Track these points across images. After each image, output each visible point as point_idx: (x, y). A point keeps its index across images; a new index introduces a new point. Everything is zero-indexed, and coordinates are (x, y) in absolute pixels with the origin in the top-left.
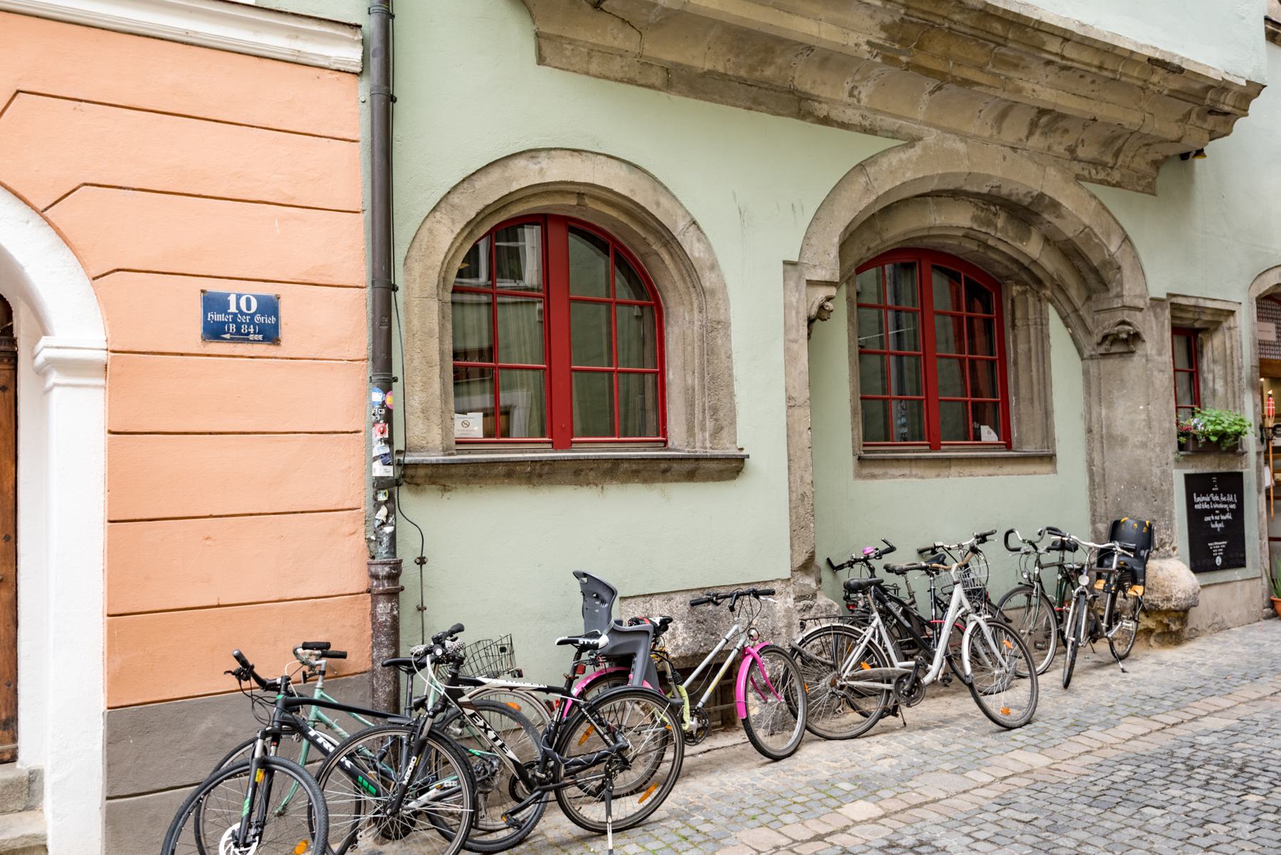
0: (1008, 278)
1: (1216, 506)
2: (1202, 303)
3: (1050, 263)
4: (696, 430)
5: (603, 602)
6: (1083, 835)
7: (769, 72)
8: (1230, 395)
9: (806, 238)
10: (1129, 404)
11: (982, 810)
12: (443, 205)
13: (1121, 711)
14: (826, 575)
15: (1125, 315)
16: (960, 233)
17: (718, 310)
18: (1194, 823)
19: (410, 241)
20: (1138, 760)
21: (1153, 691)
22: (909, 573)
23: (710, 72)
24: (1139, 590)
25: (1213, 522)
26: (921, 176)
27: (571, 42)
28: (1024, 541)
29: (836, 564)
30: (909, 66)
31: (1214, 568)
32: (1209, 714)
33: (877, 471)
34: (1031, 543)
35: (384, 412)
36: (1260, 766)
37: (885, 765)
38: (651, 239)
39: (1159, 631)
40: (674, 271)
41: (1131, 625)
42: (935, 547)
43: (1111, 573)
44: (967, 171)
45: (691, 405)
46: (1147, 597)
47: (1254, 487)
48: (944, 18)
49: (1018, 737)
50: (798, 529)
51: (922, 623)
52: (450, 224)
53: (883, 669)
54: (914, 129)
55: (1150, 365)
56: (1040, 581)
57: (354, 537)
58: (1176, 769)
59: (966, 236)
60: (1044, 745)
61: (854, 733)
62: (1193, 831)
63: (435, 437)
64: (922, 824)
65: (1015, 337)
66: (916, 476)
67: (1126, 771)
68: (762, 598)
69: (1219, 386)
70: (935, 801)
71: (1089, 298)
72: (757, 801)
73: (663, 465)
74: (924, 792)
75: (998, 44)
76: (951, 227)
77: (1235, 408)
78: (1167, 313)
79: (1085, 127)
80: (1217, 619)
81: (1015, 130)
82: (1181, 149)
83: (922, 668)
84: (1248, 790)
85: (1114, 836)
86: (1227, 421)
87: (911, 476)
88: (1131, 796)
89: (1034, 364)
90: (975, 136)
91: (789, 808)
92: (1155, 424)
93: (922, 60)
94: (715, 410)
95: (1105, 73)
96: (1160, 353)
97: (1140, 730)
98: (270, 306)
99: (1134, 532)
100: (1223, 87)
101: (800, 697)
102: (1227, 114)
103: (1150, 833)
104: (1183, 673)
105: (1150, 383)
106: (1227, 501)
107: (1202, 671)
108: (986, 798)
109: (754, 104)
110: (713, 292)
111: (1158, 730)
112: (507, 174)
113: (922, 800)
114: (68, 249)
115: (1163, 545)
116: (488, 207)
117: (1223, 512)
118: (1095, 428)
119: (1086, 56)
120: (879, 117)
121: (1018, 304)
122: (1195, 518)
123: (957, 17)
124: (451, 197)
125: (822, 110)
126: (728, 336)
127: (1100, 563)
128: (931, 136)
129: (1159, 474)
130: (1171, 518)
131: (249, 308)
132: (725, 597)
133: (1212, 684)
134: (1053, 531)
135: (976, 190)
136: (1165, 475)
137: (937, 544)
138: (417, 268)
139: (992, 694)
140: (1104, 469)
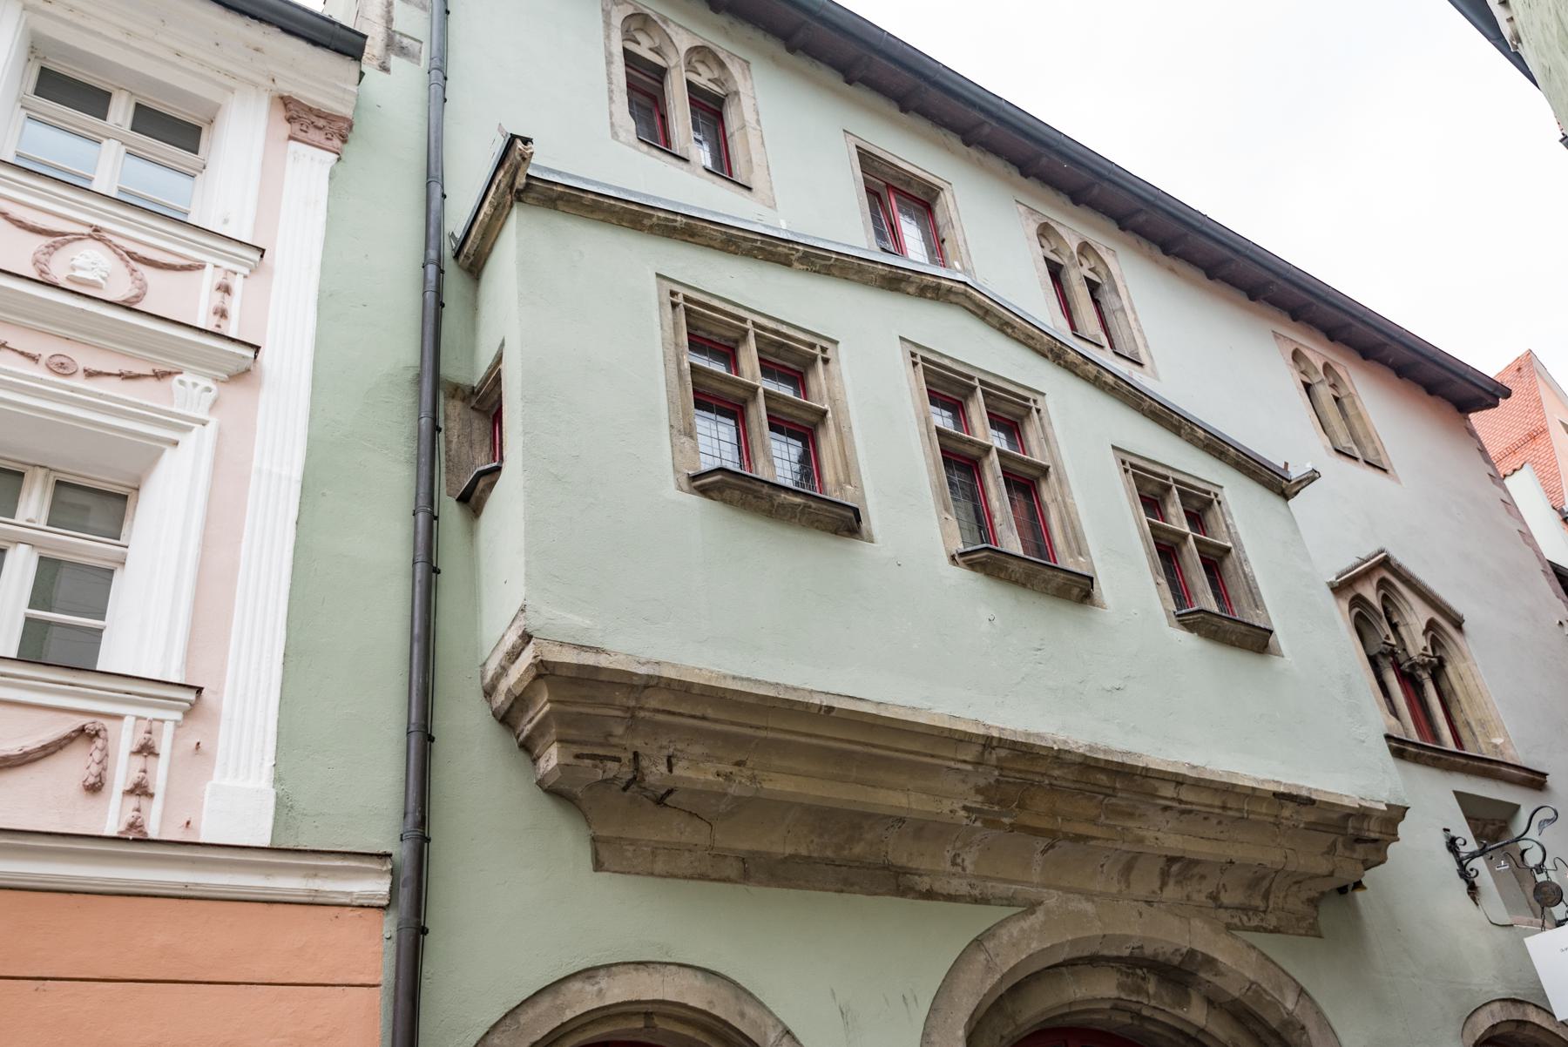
7: (858, 849)
23: (792, 857)
27: (632, 842)
30: (1013, 828)
44: (1100, 933)
48: (1043, 775)
54: (1032, 892)
59: (1114, 1008)
75: (1107, 795)
76: (1095, 1000)
79: (1222, 871)
82: (1336, 883)
90: (1101, 894)
93: (1027, 819)
95: (1230, 813)
100: (1363, 814)
102: (1375, 841)
109: (845, 886)
112: (558, 1002)
119: (1205, 798)
120: (989, 884)
123: (1056, 773)
124: (490, 1037)
125: (924, 883)
128: (1052, 899)
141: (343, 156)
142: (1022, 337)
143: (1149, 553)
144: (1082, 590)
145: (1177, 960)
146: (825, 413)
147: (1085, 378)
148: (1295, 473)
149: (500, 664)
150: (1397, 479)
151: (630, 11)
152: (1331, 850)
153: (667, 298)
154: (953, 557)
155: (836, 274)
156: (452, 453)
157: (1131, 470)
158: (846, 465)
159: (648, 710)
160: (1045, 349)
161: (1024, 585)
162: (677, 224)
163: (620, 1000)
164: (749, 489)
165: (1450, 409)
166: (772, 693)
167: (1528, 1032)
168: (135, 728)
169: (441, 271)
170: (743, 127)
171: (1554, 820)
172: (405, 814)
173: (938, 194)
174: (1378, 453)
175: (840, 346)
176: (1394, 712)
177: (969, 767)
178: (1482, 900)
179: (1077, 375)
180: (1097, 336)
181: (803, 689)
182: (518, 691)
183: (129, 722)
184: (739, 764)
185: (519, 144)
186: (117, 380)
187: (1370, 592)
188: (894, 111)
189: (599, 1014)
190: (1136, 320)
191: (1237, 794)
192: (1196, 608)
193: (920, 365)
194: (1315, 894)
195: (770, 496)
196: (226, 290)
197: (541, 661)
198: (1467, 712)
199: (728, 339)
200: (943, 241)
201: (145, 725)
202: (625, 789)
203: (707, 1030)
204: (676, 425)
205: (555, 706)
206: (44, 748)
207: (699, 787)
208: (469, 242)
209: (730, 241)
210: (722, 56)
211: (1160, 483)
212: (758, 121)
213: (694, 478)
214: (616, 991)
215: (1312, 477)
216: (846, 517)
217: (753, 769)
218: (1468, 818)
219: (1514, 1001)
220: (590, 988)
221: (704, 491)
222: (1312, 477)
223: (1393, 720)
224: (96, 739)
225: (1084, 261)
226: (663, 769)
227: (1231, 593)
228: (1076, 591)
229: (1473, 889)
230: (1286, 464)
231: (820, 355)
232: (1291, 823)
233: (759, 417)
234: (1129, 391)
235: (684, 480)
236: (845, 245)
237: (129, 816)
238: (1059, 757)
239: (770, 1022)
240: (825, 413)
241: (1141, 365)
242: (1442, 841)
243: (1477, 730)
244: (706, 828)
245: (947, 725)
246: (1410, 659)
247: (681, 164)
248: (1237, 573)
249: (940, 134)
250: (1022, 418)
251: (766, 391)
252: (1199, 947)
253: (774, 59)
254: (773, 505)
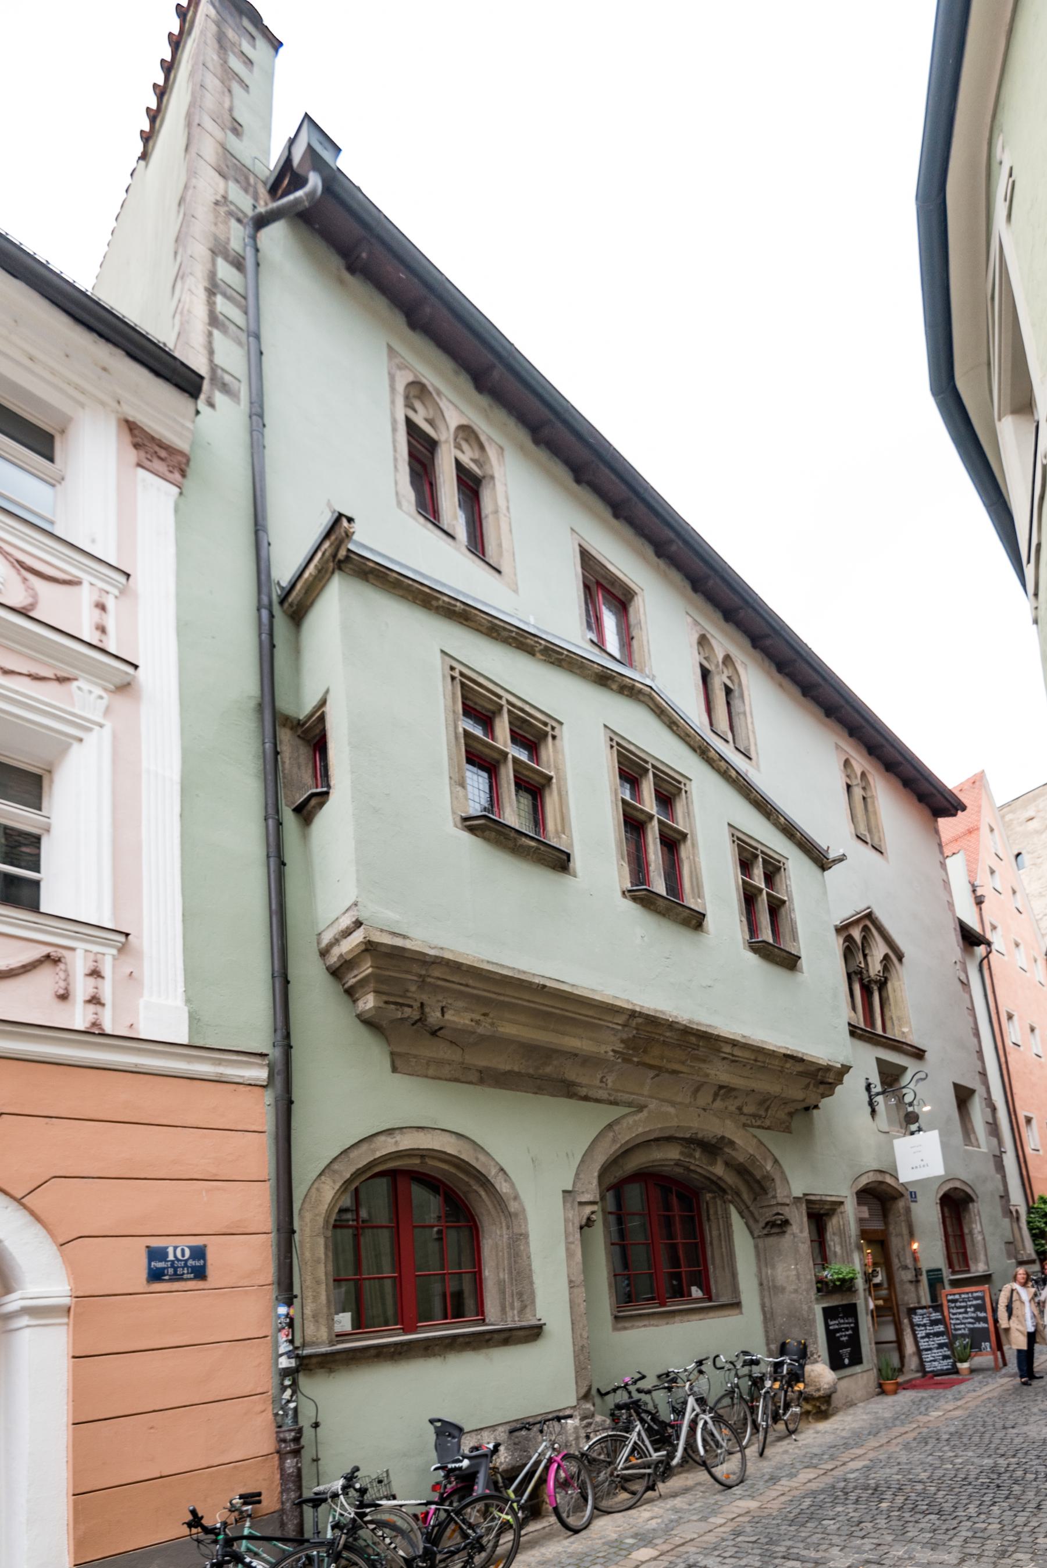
0: (703, 1189)
1: (842, 1326)
2: (824, 1198)
3: (731, 1179)
4: (508, 1309)
5: (454, 1437)
6: (789, 1543)
7: (548, 1070)
8: (845, 1254)
9: (577, 1174)
10: (785, 1265)
11: (723, 1540)
12: (326, 1171)
13: (798, 1466)
14: (598, 1400)
15: (779, 1209)
16: (672, 1163)
17: (520, 1226)
18: (853, 1524)
19: (302, 1198)
20: (814, 1493)
21: (816, 1450)
22: (654, 1393)
23: (509, 1072)
24: (801, 1386)
25: (841, 1336)
26: (648, 1129)
27: (415, 1056)
28: (726, 1362)
29: (603, 1391)
30: (639, 1064)
31: (844, 1366)
32: (852, 1460)
33: (627, 1324)
34: (732, 1363)
35: (288, 1320)
36: (886, 1485)
37: (653, 1524)
38: (472, 1182)
39: (814, 1411)
40: (488, 1203)
41: (798, 1410)
42: (669, 1372)
43: (783, 1377)
44: (676, 1125)
45: (503, 1292)
46: (806, 1390)
47: (864, 1312)
48: (660, 1035)
49: (737, 1492)
50: (580, 1369)
51: (664, 1425)
52: (332, 1184)
53: (645, 1459)
54: (642, 1100)
55: (796, 1240)
56: (738, 1388)
57: (264, 1414)
58: (838, 1496)
59: (677, 1165)
60: (755, 1494)
61: (628, 1506)
62: (853, 1529)
63: (323, 1334)
64: (687, 1555)
65: (710, 1227)
66: (653, 1325)
67: (808, 1502)
68: (563, 1421)
69: (838, 1249)
70: (692, 1540)
71: (755, 1199)
72: (571, 1561)
73: (487, 1337)
74: (684, 1536)
75: (694, 1049)
76: (667, 1160)
77: (848, 1262)
78: (804, 1206)
79: (747, 1095)
80: (849, 1399)
81: (704, 1098)
82: (804, 1105)
83: (671, 1456)
84: (881, 1501)
85: (808, 1540)
86: (845, 1271)
87: (650, 1325)
88: (814, 1516)
89: (723, 1243)
90: (680, 1103)
91: (595, 1561)
92: (802, 1277)
93: (647, 1060)
94: (520, 1294)
95: (759, 1064)
96: (801, 1231)
97: (812, 1476)
98: (199, 1253)
99: (795, 1349)
100: (828, 1069)
101: (589, 1487)
102: (830, 1083)
103: (828, 1534)
104: (833, 1436)
105: (797, 1251)
106: (846, 1322)
107: (844, 1434)
108: (724, 1533)
109: (539, 1090)
110: (516, 1215)
111: (823, 1474)
112: (372, 1147)
113: (683, 1541)
114: (39, 1226)
115: (812, 1355)
116: (358, 1170)
117: (847, 1329)
118: (765, 1282)
119: (747, 1054)
120: (619, 1094)
121: (711, 1205)
122: (831, 1335)
123: (668, 1034)
124: (332, 1165)
125: (583, 1092)
126: (527, 1244)
127: (775, 1372)
128: (653, 1105)
129: (806, 1309)
130: (816, 1337)
131: (183, 1255)
132: (534, 1424)
133: (851, 1441)
134: (746, 1353)
135: (681, 1135)
136: (811, 1310)
137: (670, 1370)
138: (308, 1216)
139: (717, 1466)
140: (772, 1309)
141: (184, 491)
142: (682, 734)
143: (739, 900)
144: (698, 922)
145: (714, 1141)
146: (551, 778)
147: (718, 770)
148: (832, 855)
149: (334, 937)
150: (887, 860)
151: (411, 379)
152: (807, 1087)
153: (448, 672)
154: (624, 893)
155: (565, 666)
156: (286, 772)
157: (737, 841)
158: (563, 819)
159: (433, 977)
160: (696, 745)
161: (664, 915)
162: (457, 609)
163: (408, 1148)
164: (502, 832)
165: (928, 813)
166: (510, 974)
167: (884, 1187)
168: (85, 958)
169: (272, 616)
170: (496, 512)
171: (924, 1079)
172: (275, 1031)
173: (633, 597)
174: (880, 841)
175: (564, 727)
176: (854, 1008)
177: (620, 1028)
178: (877, 1118)
179: (713, 768)
180: (725, 733)
181: (529, 973)
182: (349, 957)
183: (80, 953)
184: (485, 1015)
185: (345, 523)
186: (27, 680)
187: (856, 934)
188: (607, 514)
189: (396, 1155)
190: (752, 723)
191: (765, 1053)
192: (760, 939)
193: (615, 749)
194: (793, 1110)
195: (515, 839)
196: (102, 607)
197: (369, 941)
198: (893, 1012)
199: (488, 710)
200: (632, 638)
201: (91, 957)
202: (413, 1024)
203: (456, 1166)
204: (453, 777)
205: (375, 970)
206: (24, 966)
207: (459, 1027)
208: (294, 594)
209: (493, 628)
210: (483, 438)
211: (753, 852)
212: (508, 508)
213: (465, 819)
214: (406, 1142)
215: (841, 859)
216: (561, 858)
217: (492, 1019)
218: (880, 1073)
219: (881, 1172)
220: (390, 1140)
221: (471, 829)
222: (841, 859)
223: (853, 1014)
224: (59, 964)
225: (725, 670)
226: (439, 1014)
227: (781, 930)
228: (694, 922)
229: (873, 1112)
230: (828, 847)
231: (551, 732)
232: (789, 1071)
233: (508, 776)
235: (458, 819)
236: (573, 644)
237: (91, 1018)
238: (671, 1026)
239: (492, 1163)
240: (551, 778)
241: (750, 759)
242: (864, 1084)
243: (896, 1022)
244: (460, 1051)
245: (611, 1002)
246: (869, 977)
247: (449, 540)
248: (787, 917)
249: (640, 543)
250: (674, 796)
251: (514, 758)
252: (728, 1135)
253: (522, 448)
254: (516, 845)
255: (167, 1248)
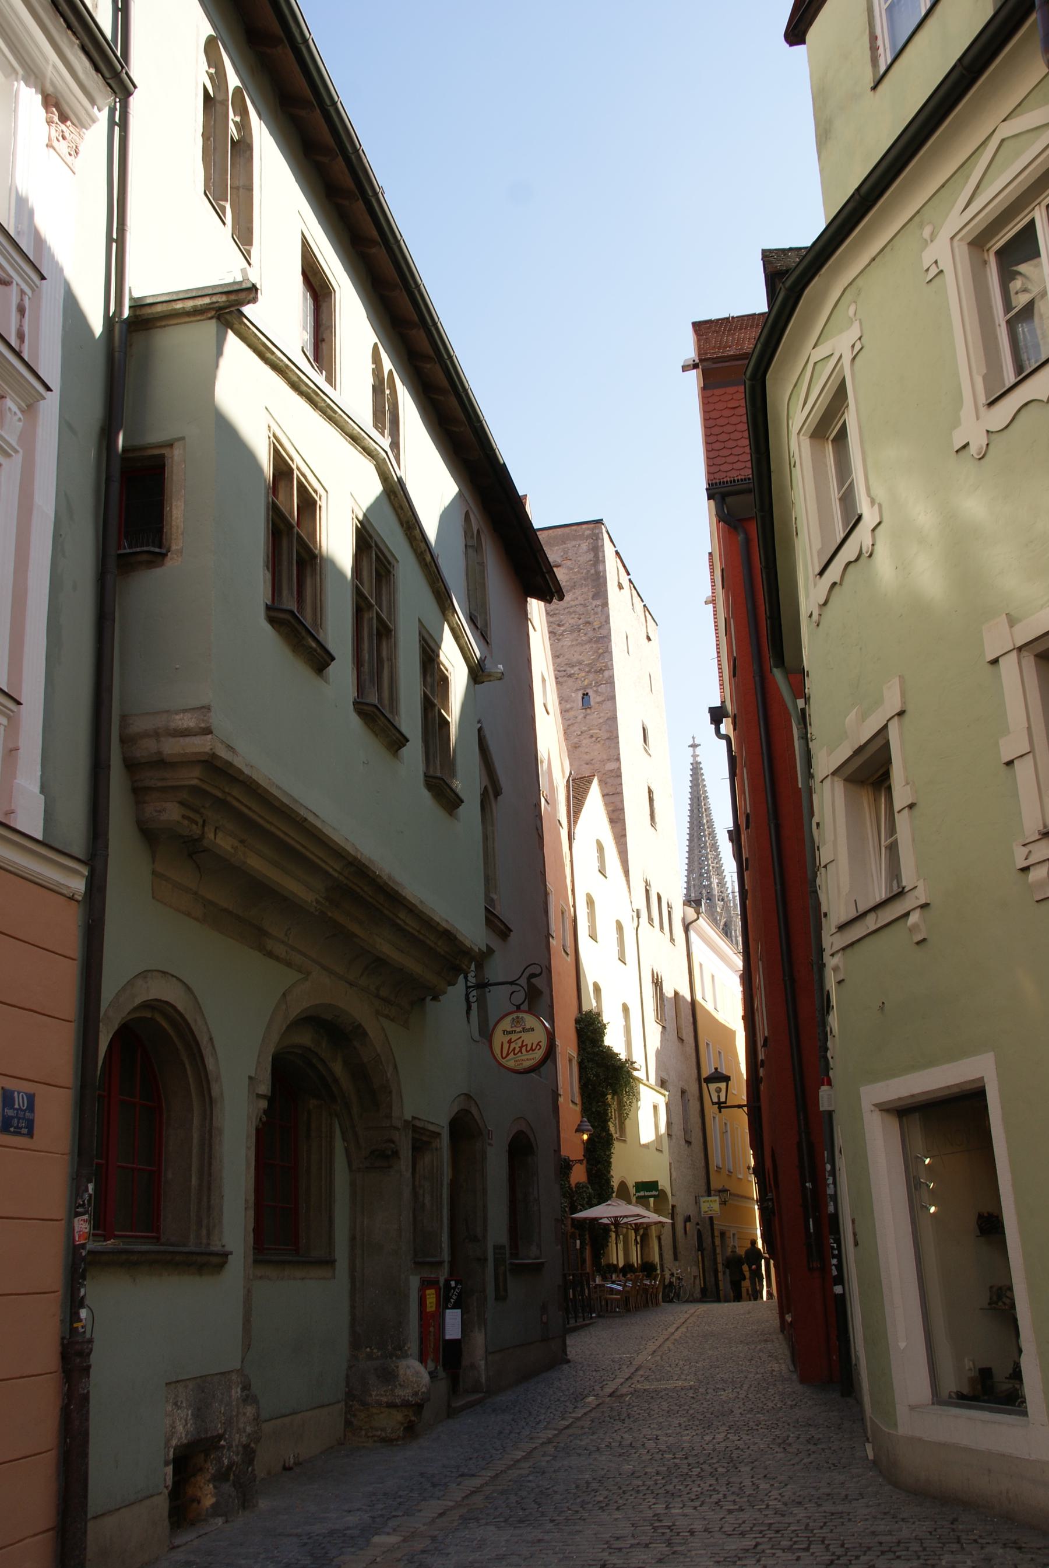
142: (397, 505)
234: (434, 572)
255: (14, 1091)
